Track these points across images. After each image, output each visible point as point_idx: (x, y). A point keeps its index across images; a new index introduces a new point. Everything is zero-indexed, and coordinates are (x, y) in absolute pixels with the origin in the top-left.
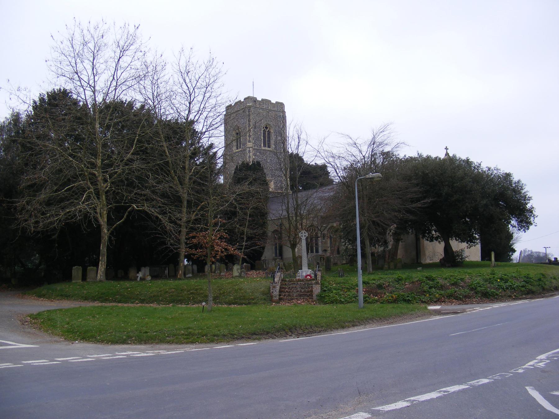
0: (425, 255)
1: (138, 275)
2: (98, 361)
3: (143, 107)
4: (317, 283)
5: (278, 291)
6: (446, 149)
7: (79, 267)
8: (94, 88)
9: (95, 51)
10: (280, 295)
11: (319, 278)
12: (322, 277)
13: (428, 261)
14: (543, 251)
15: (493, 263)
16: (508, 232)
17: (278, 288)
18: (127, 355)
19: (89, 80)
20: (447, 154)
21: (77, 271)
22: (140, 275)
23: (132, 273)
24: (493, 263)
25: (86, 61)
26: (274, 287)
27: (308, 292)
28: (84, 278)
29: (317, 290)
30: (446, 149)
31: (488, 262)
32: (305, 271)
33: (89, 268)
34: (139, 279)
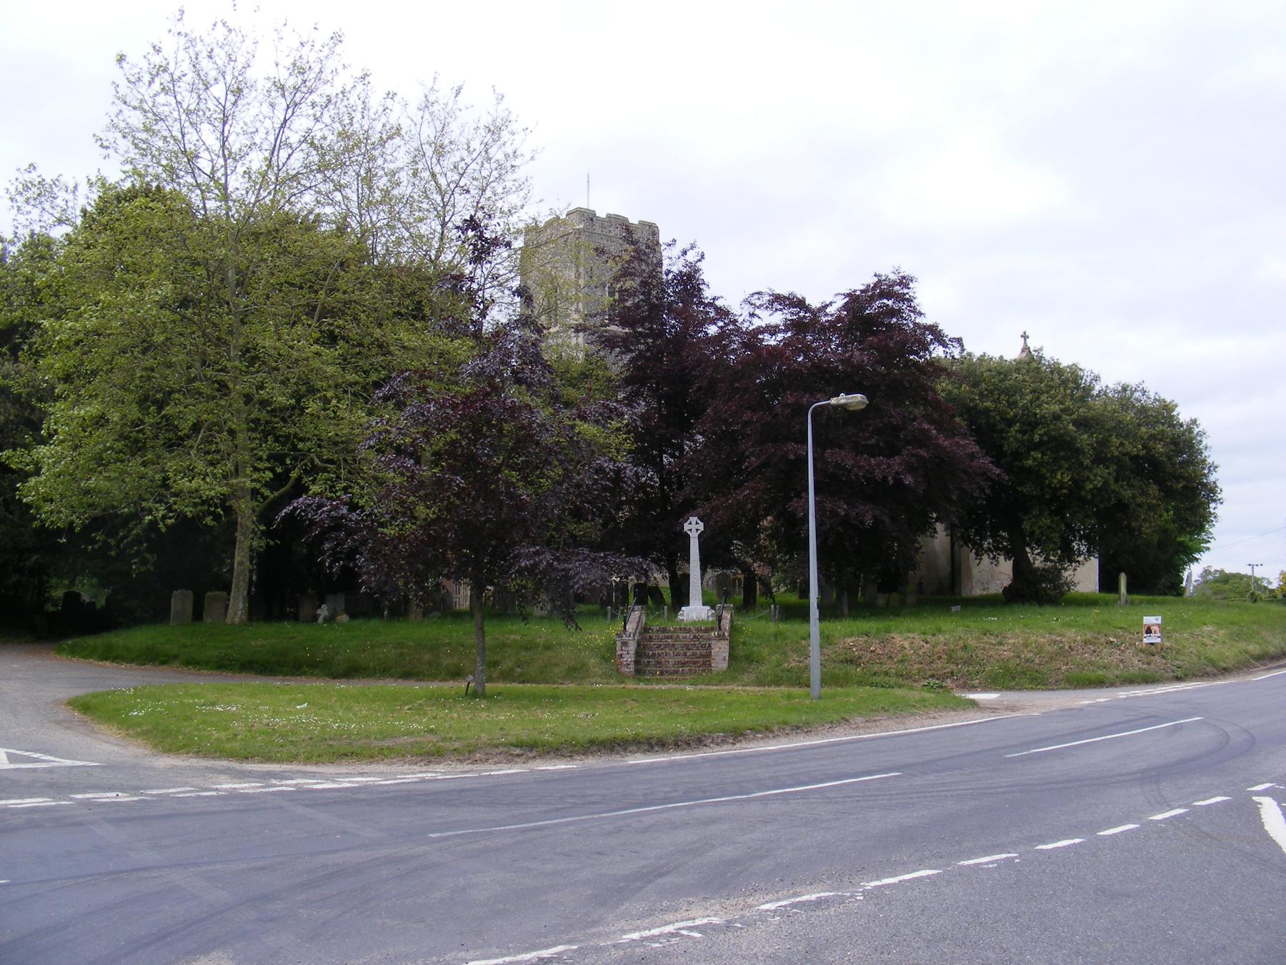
0: (970, 577)
1: (319, 611)
2: (233, 795)
3: (342, 229)
4: (721, 637)
5: (632, 652)
6: (1025, 336)
7: (186, 592)
8: (234, 166)
9: (228, 105)
10: (637, 662)
11: (726, 623)
12: (732, 621)
13: (977, 592)
14: (1246, 571)
15: (1123, 599)
16: (718, 566)
17: (632, 647)
18: (295, 785)
19: (213, 171)
20: (1026, 349)
21: (181, 601)
22: (323, 612)
23: (305, 610)
24: (1123, 599)
25: (205, 128)
26: (625, 644)
27: (702, 656)
28: (198, 615)
29: (720, 651)
30: (1025, 336)
31: (1111, 596)
32: (696, 611)
33: (209, 594)
34: (320, 620)
